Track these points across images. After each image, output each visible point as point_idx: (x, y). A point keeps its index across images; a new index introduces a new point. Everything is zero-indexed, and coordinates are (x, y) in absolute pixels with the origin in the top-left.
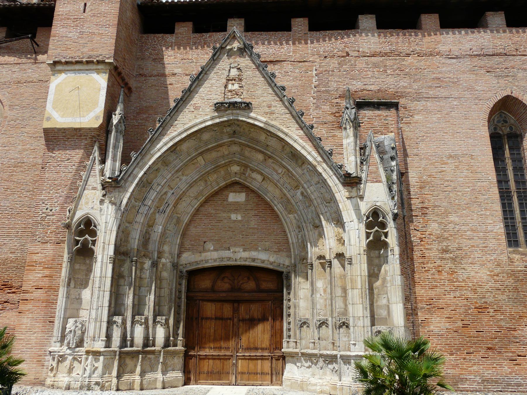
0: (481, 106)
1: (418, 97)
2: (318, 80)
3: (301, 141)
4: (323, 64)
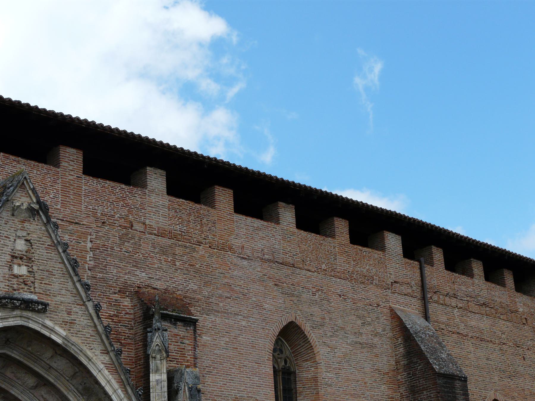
0: (267, 331)
1: (208, 311)
2: (95, 258)
3: (106, 372)
4: (100, 234)
